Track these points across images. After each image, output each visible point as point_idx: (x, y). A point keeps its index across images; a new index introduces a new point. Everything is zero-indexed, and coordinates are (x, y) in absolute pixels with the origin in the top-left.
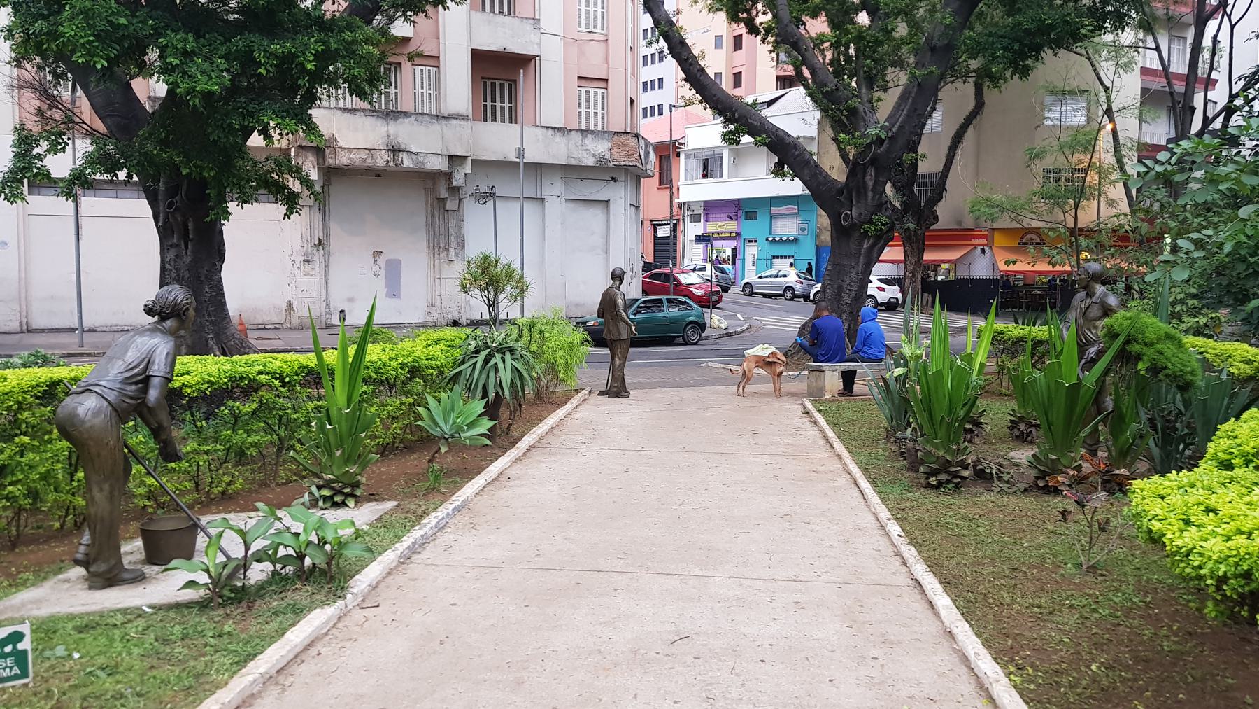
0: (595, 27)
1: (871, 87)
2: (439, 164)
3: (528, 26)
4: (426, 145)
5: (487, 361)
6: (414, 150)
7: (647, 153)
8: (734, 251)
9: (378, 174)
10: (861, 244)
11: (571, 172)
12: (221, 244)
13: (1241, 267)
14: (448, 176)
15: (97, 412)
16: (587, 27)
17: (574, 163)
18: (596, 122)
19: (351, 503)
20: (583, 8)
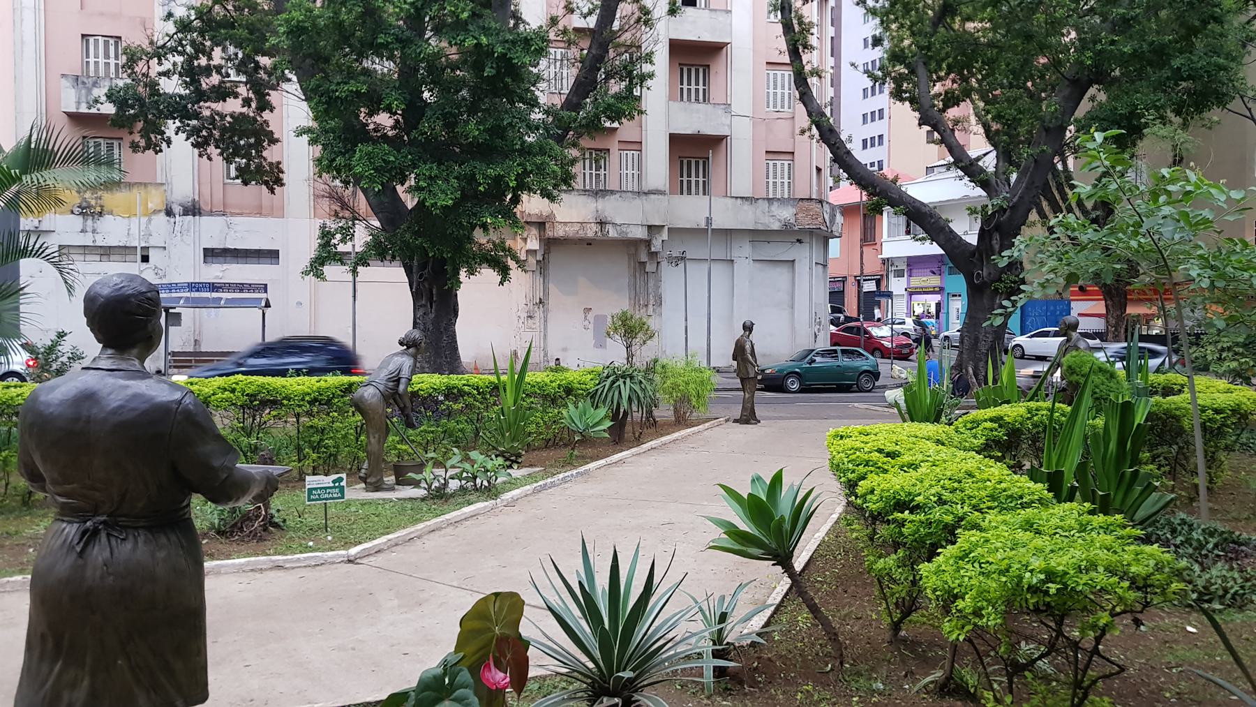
0: (783, 107)
2: (640, 233)
3: (720, 111)
4: (628, 217)
5: (613, 382)
6: (618, 222)
7: (833, 217)
8: (938, 305)
9: (589, 242)
11: (758, 236)
14: (648, 243)
15: (375, 395)
16: (775, 106)
17: (761, 228)
18: (783, 191)
19: (515, 466)
20: (771, 91)
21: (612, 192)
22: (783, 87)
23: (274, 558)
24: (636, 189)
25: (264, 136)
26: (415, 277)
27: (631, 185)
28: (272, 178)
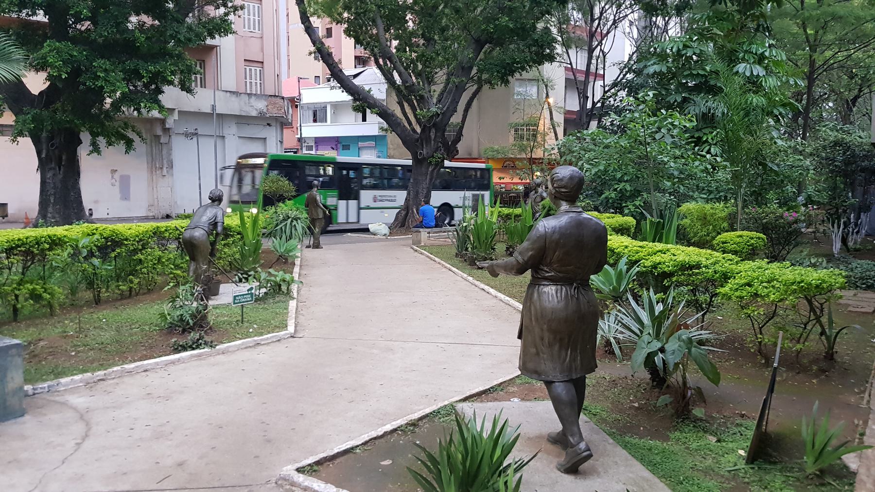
0: (254, 29)
1: (429, 83)
10: (428, 168)
11: (242, 120)
12: (78, 167)
13: (599, 181)
15: (203, 235)
16: (249, 28)
22: (254, 15)
23: (256, 338)
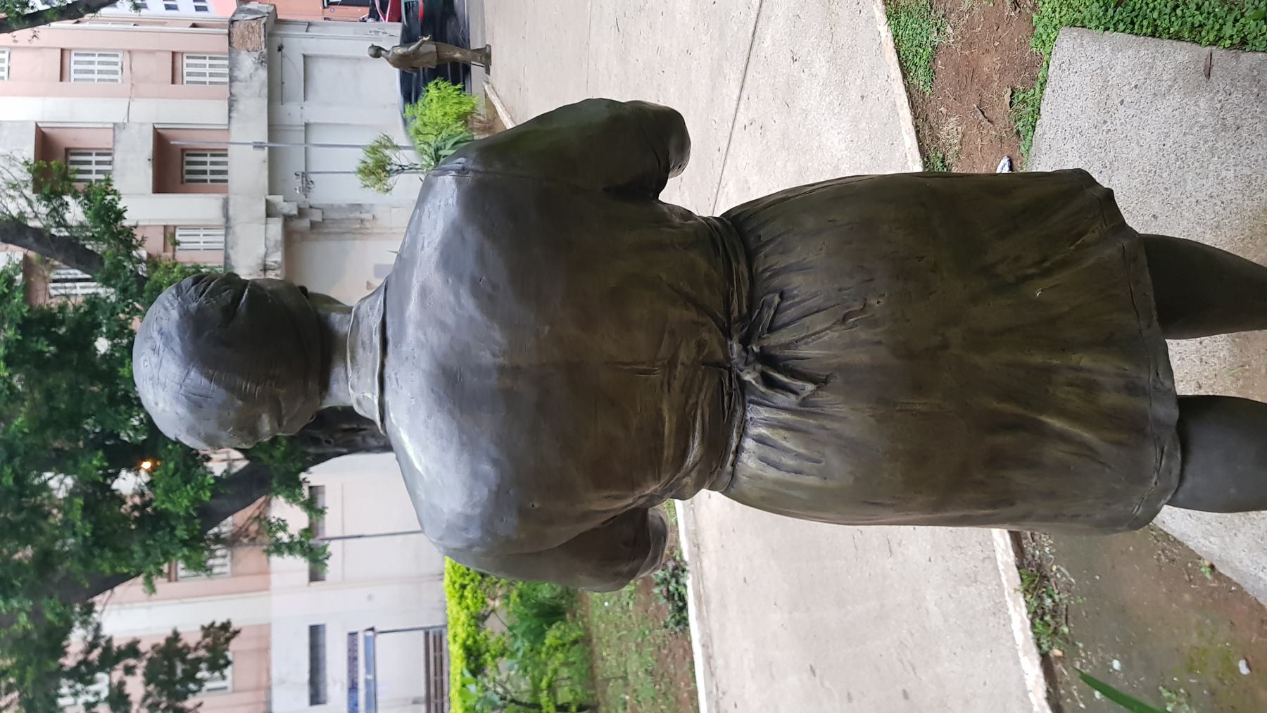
0: (116, 64)
2: (276, 227)
3: (122, 136)
6: (262, 251)
7: (250, 11)
11: (275, 94)
14: (287, 219)
16: (115, 73)
17: (265, 91)
18: (220, 66)
20: (96, 76)
21: (227, 258)
22: (91, 63)
24: (223, 232)
25: (172, 649)
26: (330, 450)
27: (218, 237)
28: (220, 637)
